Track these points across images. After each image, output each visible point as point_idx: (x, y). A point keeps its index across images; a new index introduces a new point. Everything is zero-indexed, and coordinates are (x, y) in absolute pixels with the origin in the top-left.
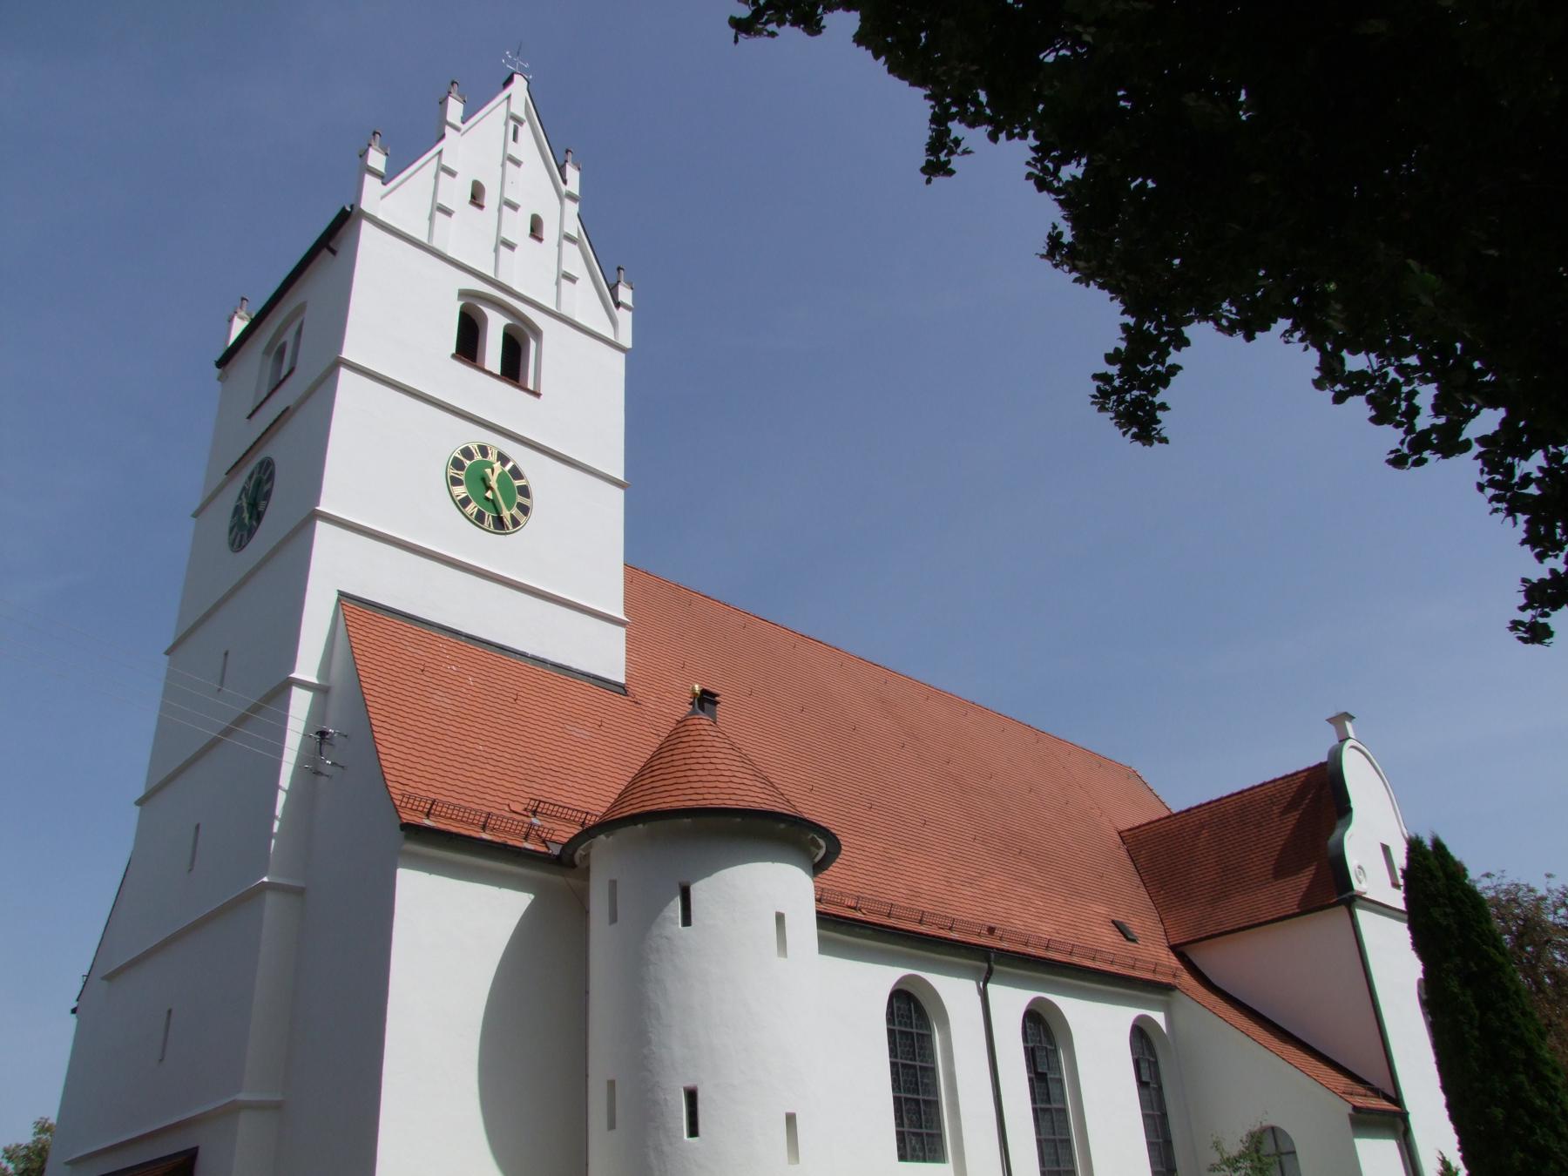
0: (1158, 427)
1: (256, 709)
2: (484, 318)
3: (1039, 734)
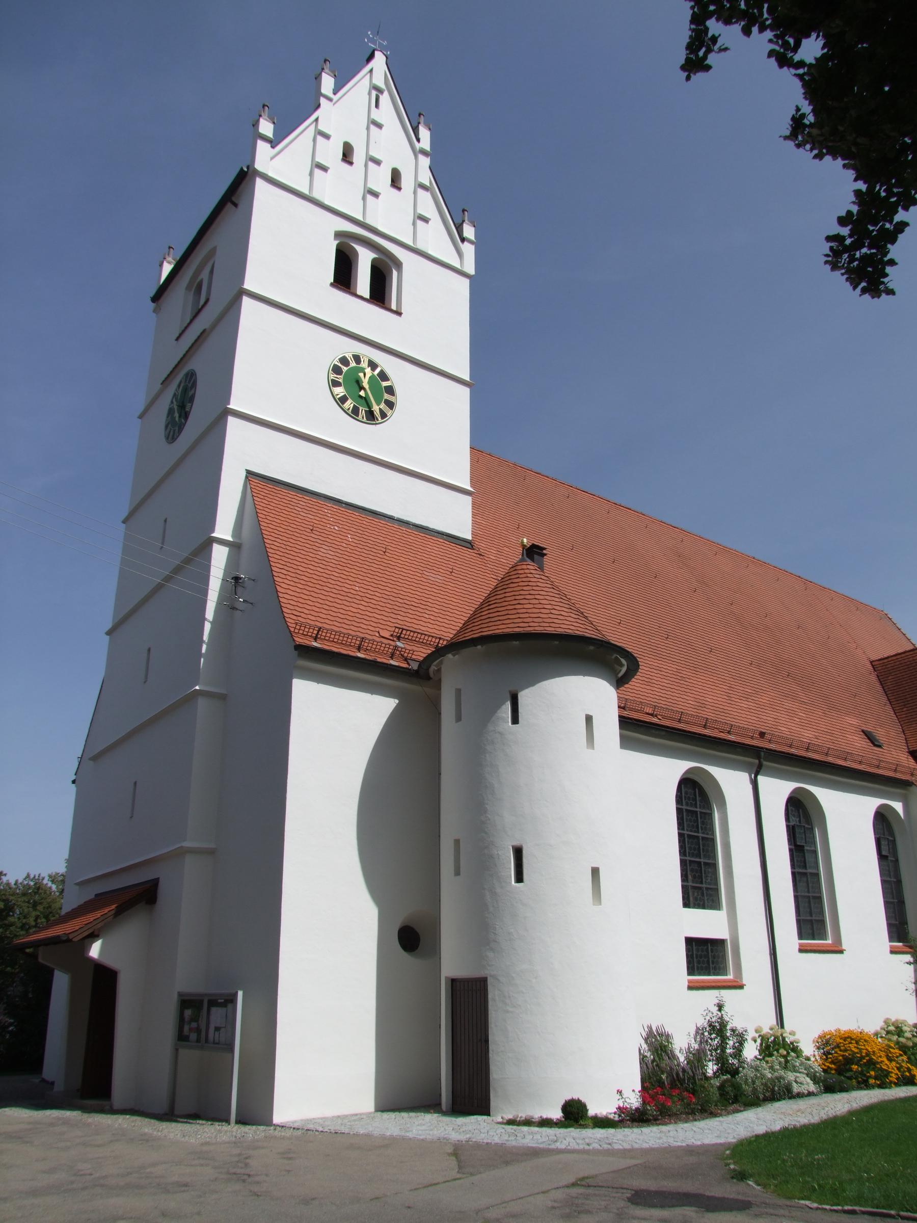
0: (885, 280)
1: (188, 561)
2: (356, 254)
3: (807, 582)
